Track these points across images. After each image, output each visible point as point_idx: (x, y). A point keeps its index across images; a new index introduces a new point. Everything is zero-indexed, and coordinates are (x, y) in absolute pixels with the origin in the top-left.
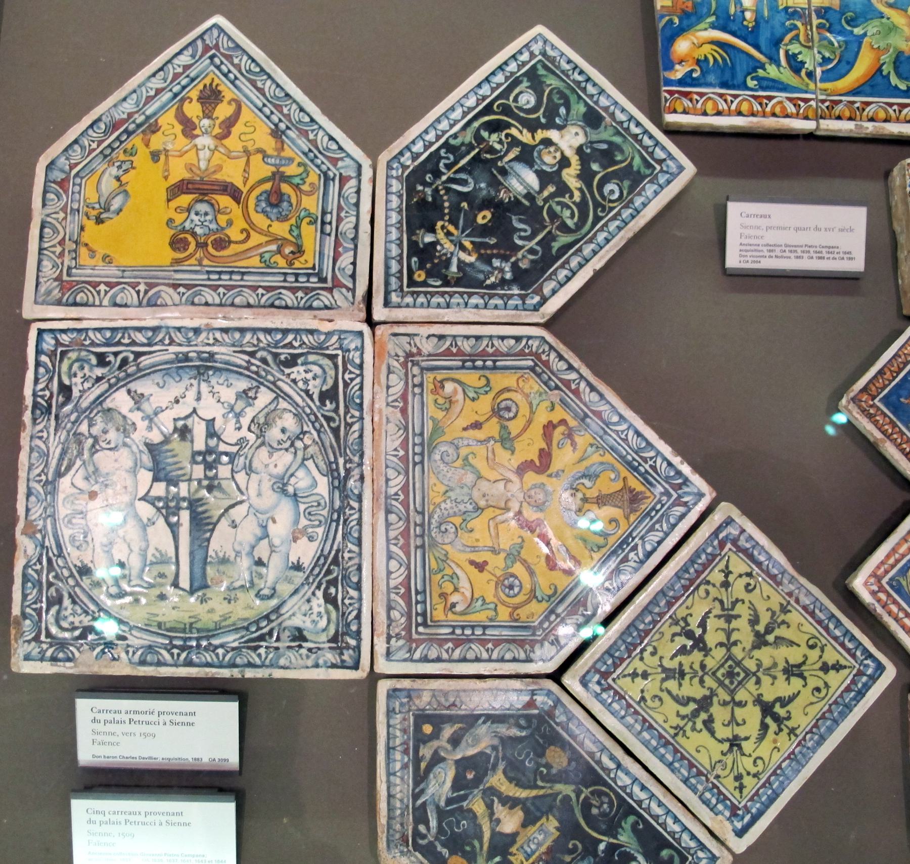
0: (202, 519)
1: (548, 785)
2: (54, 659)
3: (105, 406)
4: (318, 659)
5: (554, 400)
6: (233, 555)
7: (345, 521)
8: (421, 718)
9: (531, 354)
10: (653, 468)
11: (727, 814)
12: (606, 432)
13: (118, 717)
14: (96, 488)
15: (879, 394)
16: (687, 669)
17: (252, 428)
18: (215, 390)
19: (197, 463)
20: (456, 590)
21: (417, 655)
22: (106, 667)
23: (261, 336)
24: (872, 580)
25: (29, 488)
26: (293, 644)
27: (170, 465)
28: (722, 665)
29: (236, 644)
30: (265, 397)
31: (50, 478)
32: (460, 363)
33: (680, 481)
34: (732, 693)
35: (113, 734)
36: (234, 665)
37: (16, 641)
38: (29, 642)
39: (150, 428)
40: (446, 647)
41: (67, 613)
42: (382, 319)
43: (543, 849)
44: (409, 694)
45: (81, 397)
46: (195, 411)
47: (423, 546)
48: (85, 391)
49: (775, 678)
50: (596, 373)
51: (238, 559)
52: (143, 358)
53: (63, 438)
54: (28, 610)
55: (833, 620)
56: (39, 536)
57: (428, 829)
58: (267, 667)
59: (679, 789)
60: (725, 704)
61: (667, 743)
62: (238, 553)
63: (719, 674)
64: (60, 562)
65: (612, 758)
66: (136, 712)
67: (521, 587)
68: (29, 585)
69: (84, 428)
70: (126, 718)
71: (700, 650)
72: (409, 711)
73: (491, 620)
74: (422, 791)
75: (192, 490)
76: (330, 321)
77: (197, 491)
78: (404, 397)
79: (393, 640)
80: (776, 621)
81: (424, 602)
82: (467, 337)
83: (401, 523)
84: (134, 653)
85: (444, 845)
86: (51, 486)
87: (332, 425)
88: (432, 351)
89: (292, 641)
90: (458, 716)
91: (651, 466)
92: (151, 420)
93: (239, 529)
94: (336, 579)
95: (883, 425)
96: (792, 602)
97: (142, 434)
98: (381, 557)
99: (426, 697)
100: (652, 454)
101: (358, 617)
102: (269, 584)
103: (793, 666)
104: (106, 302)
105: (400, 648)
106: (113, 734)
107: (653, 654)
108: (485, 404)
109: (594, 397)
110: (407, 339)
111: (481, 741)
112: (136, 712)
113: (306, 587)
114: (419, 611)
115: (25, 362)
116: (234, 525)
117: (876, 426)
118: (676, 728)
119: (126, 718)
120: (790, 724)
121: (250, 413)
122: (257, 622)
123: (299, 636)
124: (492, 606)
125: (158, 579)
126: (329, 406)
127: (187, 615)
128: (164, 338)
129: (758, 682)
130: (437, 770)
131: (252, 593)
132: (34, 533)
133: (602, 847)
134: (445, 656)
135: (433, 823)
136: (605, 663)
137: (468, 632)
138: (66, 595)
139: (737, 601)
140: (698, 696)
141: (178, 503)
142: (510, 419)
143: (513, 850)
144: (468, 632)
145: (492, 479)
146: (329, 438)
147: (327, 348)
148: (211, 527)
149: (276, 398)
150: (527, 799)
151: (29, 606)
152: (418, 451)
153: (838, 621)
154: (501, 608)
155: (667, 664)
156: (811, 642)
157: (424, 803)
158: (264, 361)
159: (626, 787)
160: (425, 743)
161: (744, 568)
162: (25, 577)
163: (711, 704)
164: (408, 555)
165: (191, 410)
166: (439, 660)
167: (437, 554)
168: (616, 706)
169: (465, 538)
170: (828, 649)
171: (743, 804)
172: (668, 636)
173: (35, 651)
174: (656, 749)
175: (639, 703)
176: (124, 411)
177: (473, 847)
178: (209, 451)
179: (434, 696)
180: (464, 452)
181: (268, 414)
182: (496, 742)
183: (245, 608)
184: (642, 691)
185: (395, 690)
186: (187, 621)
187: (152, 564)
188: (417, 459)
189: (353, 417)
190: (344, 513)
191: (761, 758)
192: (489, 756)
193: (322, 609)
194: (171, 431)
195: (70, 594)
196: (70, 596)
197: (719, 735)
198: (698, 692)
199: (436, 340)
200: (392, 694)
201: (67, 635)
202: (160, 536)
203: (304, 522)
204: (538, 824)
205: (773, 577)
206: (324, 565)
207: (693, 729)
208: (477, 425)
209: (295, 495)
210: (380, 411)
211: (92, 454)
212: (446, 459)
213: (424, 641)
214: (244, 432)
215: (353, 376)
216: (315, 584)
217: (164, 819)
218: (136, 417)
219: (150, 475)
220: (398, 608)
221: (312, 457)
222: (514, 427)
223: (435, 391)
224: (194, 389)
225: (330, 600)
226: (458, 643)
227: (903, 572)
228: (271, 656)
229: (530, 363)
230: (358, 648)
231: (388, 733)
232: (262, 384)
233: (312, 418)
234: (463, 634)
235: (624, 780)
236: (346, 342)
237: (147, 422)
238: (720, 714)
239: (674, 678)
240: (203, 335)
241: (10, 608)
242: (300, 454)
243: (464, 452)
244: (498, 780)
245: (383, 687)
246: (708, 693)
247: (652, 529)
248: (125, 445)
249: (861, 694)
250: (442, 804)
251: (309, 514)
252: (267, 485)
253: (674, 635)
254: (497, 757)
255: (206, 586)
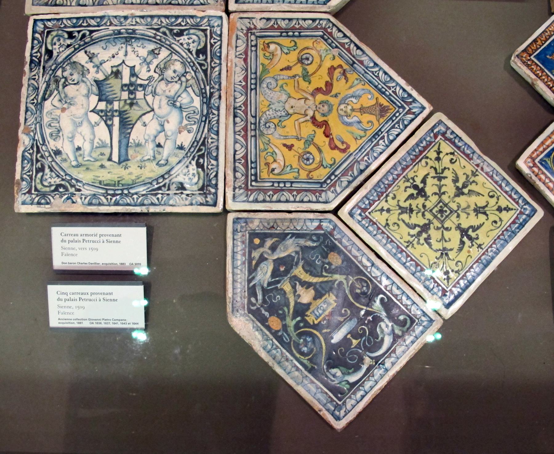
0: (126, 122)
1: (330, 275)
2: (39, 203)
3: (72, 61)
4: (192, 200)
5: (334, 53)
6: (144, 142)
7: (209, 121)
8: (253, 235)
9: (321, 28)
10: (395, 92)
11: (440, 294)
12: (366, 72)
13: (76, 238)
14: (65, 106)
15: (533, 54)
16: (414, 207)
17: (157, 71)
18: (135, 50)
19: (124, 91)
20: (275, 161)
21: (251, 199)
22: (69, 207)
23: (163, 20)
24: (529, 160)
25: (27, 108)
26: (178, 192)
27: (108, 92)
28: (436, 206)
29: (144, 192)
30: (164, 53)
31: (39, 101)
32: (279, 34)
33: (411, 100)
34: (442, 222)
35: (73, 249)
36: (143, 205)
37: (17, 194)
38: (25, 194)
39: (97, 72)
40: (268, 194)
41: (47, 177)
42: (234, 10)
43: (327, 313)
44: (246, 221)
45: (58, 56)
46: (123, 62)
47: (255, 136)
48: (60, 52)
49: (468, 214)
50: (361, 40)
51: (147, 144)
52: (94, 34)
53: (47, 79)
54: (25, 176)
55: (505, 181)
56: (32, 134)
57: (257, 300)
58: (162, 205)
59: (410, 279)
60: (438, 228)
61: (402, 251)
62: (146, 141)
63: (434, 211)
64: (44, 148)
65: (369, 260)
66: (87, 235)
67: (314, 159)
68: (26, 161)
69: (59, 73)
70: (81, 238)
71: (422, 196)
72: (246, 230)
73: (296, 178)
74: (253, 278)
75: (121, 106)
76: (203, 11)
77: (123, 107)
78: (246, 53)
79: (237, 190)
80: (469, 181)
81: (256, 168)
82: (284, 19)
83: (243, 123)
84: (85, 198)
85: (266, 310)
86: (39, 106)
87: (203, 68)
88: (263, 27)
89: (177, 190)
90: (275, 233)
91: (393, 91)
92: (98, 67)
93: (148, 127)
94: (203, 154)
95: (536, 71)
96: (479, 170)
97: (93, 75)
98: (231, 141)
99: (256, 223)
100: (394, 84)
101: (216, 176)
102: (164, 158)
103: (480, 208)
104: (73, 4)
105: (241, 194)
106: (73, 249)
107: (394, 198)
108: (293, 57)
109: (359, 52)
110: (248, 20)
111: (290, 248)
112: (87, 235)
113: (186, 159)
114: (253, 173)
115: (27, 38)
116: (145, 125)
117: (532, 71)
118: (407, 242)
119: (81, 238)
120: (479, 242)
121: (156, 62)
122: (157, 179)
123: (181, 187)
124: (296, 170)
125: (100, 157)
126: (202, 57)
127: (116, 176)
128: (107, 22)
129: (458, 216)
130: (262, 265)
131: (154, 163)
132: (29, 132)
133: (363, 313)
134: (268, 199)
135: (260, 297)
136: (364, 203)
137: (282, 185)
138: (47, 167)
139: (445, 168)
140: (421, 224)
141: (113, 113)
142: (308, 65)
143: (308, 313)
144: (282, 185)
145: (297, 98)
146: (201, 75)
147: (201, 26)
148: (131, 126)
149: (171, 54)
150: (316, 283)
151: (25, 174)
152: (253, 82)
153: (508, 182)
154: (301, 171)
155: (402, 204)
156: (491, 194)
157: (254, 285)
158: (164, 33)
159: (377, 277)
160: (255, 249)
161: (449, 150)
162: (23, 156)
163: (429, 228)
164: (246, 140)
165: (121, 61)
166: (264, 201)
167: (264, 141)
168: (370, 228)
169: (280, 131)
170: (501, 198)
171: (449, 289)
172: (403, 188)
173: (27, 198)
174: (395, 254)
175: (385, 227)
176: (83, 63)
177: (284, 311)
178: (131, 84)
179: (261, 222)
180: (280, 83)
181: (166, 63)
182: (298, 249)
183: (150, 172)
184: (387, 220)
185: (238, 218)
186: (116, 180)
187: (97, 147)
188: (253, 87)
189: (215, 63)
190: (209, 117)
191: (461, 262)
192: (294, 257)
193: (195, 172)
194: (109, 73)
195: (49, 166)
196: (49, 167)
197: (434, 247)
198: (422, 222)
199: (265, 21)
200: (236, 221)
201: (47, 189)
202: (102, 131)
203: (185, 122)
204: (323, 298)
205: (467, 156)
206: (196, 146)
207: (418, 243)
208: (288, 68)
209: (181, 107)
210: (231, 61)
211: (64, 87)
212: (270, 87)
213: (256, 190)
214: (152, 73)
215: (216, 41)
216: (191, 157)
217: (101, 297)
218: (89, 66)
219: (97, 98)
220: (240, 171)
221: (191, 86)
222: (311, 69)
223: (264, 49)
224: (124, 50)
225: (199, 165)
226: (276, 191)
227: (548, 155)
228: (165, 198)
229: (321, 33)
230: (216, 194)
231: (233, 244)
232: (163, 46)
233: (192, 64)
234: (279, 186)
235: (376, 273)
236: (212, 22)
237: (96, 68)
238: (435, 234)
239: (407, 213)
240: (130, 20)
241: (15, 175)
242: (184, 84)
243: (280, 83)
244: (299, 271)
245: (231, 217)
246: (427, 222)
247: (393, 127)
248: (83, 81)
249: (522, 225)
250: (265, 285)
251: (189, 117)
252: (164, 101)
253: (406, 187)
254: (298, 258)
255: (128, 160)
